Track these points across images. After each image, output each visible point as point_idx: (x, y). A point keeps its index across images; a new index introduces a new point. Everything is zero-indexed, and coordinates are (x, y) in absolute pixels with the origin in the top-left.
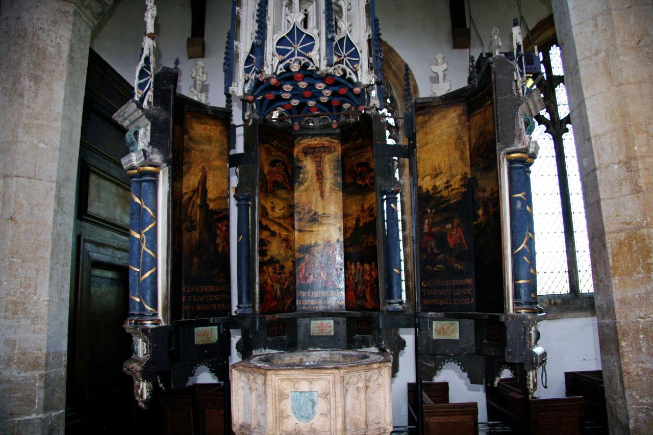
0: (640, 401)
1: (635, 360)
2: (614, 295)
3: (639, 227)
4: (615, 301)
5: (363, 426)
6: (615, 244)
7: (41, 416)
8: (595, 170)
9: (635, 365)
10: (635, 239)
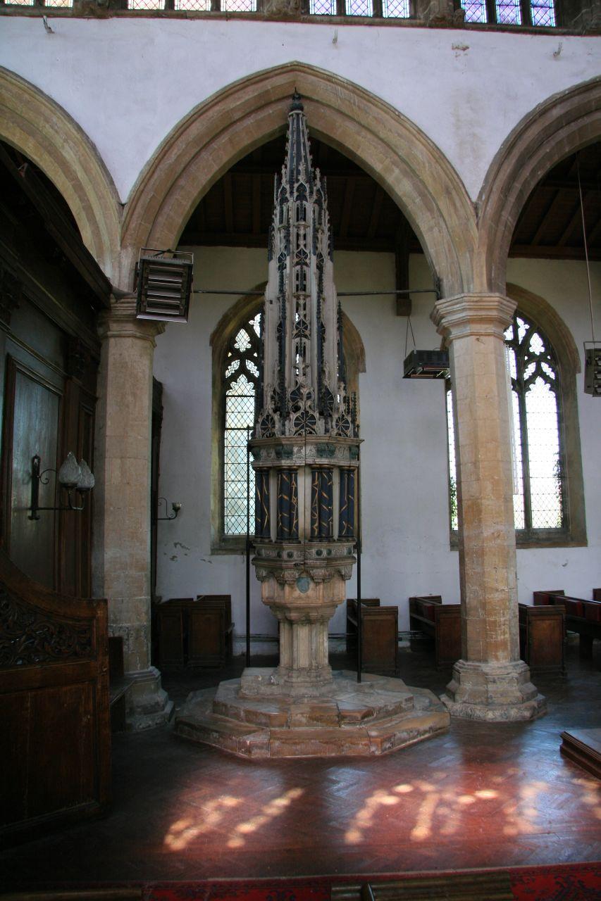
5: (332, 596)
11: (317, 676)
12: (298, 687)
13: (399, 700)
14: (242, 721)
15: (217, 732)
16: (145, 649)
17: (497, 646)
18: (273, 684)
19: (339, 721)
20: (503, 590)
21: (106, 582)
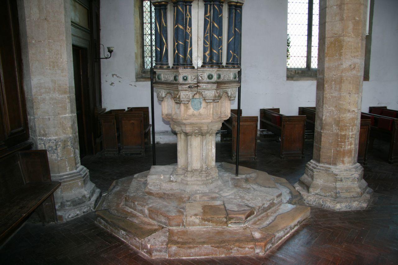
0: (328, 109)
1: (329, 92)
2: (325, 65)
3: (340, 36)
4: (325, 68)
5: (220, 113)
6: (329, 43)
7: (70, 115)
8: (326, 8)
9: (329, 94)
10: (338, 41)
11: (207, 176)
12: (192, 185)
13: (272, 197)
14: (146, 217)
15: (124, 230)
16: (72, 155)
17: (344, 154)
18: (172, 181)
19: (227, 222)
20: (354, 111)
21: (35, 104)
